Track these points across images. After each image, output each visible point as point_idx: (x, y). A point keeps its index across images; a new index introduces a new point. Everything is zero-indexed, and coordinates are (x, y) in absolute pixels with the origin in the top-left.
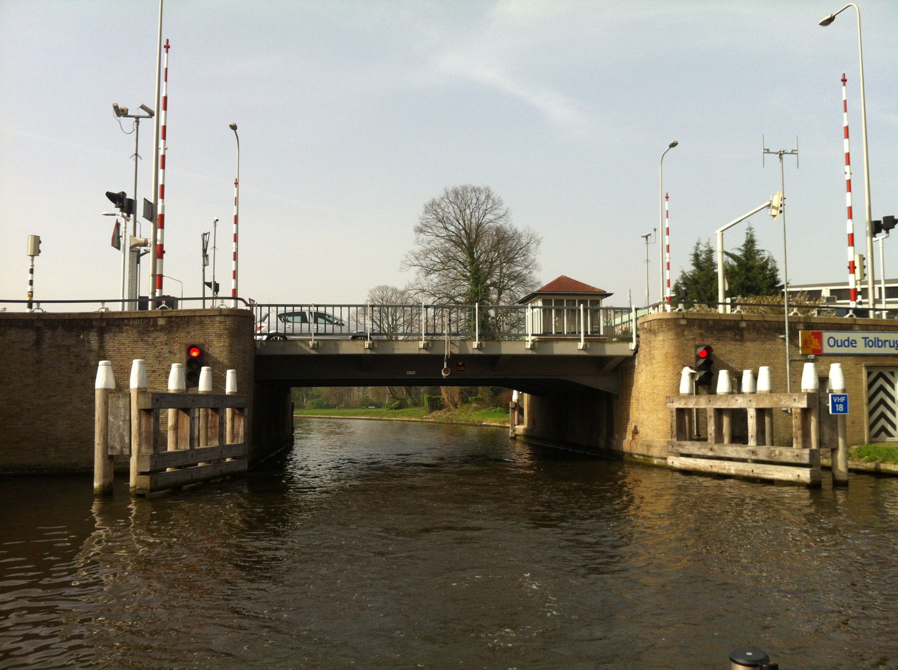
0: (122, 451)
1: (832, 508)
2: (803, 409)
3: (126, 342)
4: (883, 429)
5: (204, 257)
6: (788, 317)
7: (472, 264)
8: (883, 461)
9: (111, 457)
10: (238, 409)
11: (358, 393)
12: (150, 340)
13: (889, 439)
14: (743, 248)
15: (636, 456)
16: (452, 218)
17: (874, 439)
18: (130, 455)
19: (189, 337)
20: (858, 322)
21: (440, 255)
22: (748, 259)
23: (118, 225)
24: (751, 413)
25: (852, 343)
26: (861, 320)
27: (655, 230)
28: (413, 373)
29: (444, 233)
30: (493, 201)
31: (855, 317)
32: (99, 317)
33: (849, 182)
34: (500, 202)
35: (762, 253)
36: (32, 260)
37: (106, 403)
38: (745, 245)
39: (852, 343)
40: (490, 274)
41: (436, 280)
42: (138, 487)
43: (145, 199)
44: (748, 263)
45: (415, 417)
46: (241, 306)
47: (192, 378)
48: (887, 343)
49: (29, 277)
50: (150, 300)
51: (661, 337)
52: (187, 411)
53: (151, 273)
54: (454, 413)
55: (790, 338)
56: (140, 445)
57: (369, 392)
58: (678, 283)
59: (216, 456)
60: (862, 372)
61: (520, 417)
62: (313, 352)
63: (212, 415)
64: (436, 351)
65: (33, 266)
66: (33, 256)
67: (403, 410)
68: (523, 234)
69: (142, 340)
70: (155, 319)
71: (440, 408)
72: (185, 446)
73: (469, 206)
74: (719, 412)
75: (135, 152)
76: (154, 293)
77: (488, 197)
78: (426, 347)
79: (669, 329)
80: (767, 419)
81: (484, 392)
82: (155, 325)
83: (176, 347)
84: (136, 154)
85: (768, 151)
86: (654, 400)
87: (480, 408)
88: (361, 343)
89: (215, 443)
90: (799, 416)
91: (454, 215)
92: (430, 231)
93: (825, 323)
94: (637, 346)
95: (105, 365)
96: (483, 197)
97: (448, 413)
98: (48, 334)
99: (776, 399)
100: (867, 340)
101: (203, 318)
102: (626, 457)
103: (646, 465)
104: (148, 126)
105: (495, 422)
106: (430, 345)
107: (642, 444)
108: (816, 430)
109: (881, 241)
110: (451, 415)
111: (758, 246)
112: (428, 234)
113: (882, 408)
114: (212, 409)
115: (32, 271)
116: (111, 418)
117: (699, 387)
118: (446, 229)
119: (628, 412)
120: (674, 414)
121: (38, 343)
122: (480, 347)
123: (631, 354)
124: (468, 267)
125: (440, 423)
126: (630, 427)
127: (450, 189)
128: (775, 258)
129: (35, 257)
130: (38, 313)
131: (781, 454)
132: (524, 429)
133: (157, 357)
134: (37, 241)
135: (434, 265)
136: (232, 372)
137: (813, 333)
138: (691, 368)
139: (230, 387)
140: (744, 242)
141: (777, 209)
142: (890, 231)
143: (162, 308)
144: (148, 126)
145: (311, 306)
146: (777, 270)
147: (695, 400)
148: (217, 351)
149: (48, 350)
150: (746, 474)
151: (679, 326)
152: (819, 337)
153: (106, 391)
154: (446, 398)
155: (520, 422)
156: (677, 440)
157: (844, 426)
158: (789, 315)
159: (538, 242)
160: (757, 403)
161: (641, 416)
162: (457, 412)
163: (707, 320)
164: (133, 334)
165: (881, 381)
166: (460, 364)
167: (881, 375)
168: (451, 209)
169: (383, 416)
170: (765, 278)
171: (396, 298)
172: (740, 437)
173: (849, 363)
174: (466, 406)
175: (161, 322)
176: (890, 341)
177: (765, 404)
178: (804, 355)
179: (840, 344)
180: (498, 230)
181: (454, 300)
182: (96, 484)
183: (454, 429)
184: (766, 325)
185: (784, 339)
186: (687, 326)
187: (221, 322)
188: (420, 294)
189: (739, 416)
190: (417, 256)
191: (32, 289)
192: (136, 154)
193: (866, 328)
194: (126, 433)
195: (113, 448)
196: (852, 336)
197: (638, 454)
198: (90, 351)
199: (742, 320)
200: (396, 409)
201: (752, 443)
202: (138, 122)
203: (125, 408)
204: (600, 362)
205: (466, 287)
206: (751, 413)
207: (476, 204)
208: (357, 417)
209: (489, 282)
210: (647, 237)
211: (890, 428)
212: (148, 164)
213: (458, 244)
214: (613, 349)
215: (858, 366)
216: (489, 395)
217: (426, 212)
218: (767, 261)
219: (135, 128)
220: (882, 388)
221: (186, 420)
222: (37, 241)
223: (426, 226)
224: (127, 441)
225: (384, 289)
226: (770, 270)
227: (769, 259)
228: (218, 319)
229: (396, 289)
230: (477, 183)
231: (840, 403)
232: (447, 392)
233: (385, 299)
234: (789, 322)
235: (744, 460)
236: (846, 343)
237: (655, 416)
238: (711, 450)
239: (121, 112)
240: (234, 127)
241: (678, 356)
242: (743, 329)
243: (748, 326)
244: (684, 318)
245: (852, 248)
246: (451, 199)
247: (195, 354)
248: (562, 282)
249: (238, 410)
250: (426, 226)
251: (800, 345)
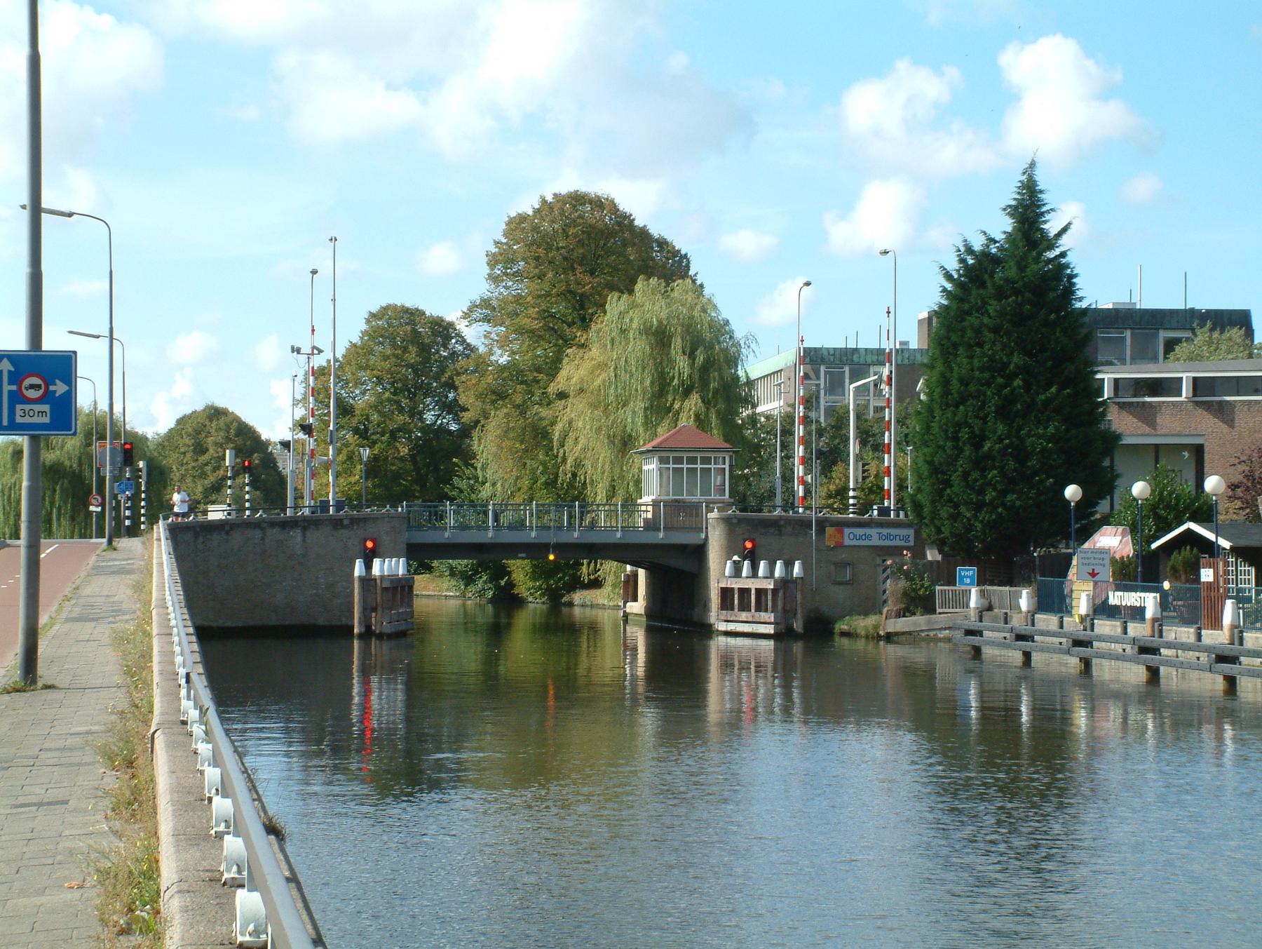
25: (868, 537)
39: (868, 537)
69: (333, 536)
123: (702, 542)
147: (480, 620)
152: (842, 533)
172: (744, 607)
196: (868, 531)
231: (967, 577)
236: (864, 537)
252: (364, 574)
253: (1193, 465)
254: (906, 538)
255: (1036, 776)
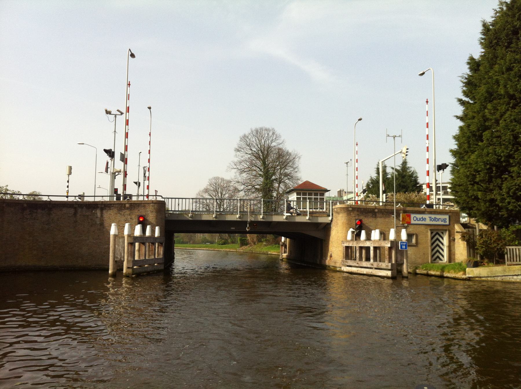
0: (121, 259)
1: (400, 286)
2: (389, 247)
3: (112, 214)
4: (438, 257)
5: (144, 177)
6: (396, 208)
7: (264, 168)
8: (430, 270)
9: (116, 261)
10: (160, 243)
11: (199, 236)
12: (122, 213)
13: (440, 262)
14: (401, 166)
15: (331, 267)
16: (254, 144)
17: (434, 261)
18: (124, 260)
19: (139, 212)
20: (427, 210)
21: (248, 164)
22: (403, 172)
23: (107, 163)
24: (372, 249)
25: (424, 219)
26: (429, 210)
27: (351, 160)
28: (234, 228)
29: (250, 152)
30: (276, 135)
31: (426, 208)
32: (101, 203)
33: (428, 148)
34: (280, 136)
35: (411, 168)
36: (69, 177)
37: (115, 240)
38: (402, 164)
39: (424, 219)
40: (274, 174)
41: (246, 176)
42: (127, 273)
43: (121, 153)
44: (403, 173)
45: (233, 249)
46: (159, 199)
47: (144, 230)
48: (440, 220)
49: (67, 184)
50: (122, 196)
51: (341, 215)
52: (144, 244)
53: (122, 184)
54: (254, 247)
55: (396, 216)
56: (128, 257)
57: (207, 236)
58: (369, 182)
59: (151, 262)
60: (428, 232)
61: (285, 249)
62: (191, 219)
63: (151, 246)
64: (244, 219)
65: (69, 179)
66: (69, 175)
67: (227, 245)
68: (292, 153)
69: (119, 213)
70: (125, 204)
71: (247, 244)
72: (142, 258)
73: (263, 138)
74: (361, 248)
75: (114, 130)
76: (123, 193)
77: (273, 133)
78: (240, 218)
79: (344, 212)
80: (378, 251)
81: (270, 237)
82: (125, 207)
83: (133, 216)
84: (115, 131)
85: (389, 136)
86: (338, 243)
87: (267, 245)
88: (212, 215)
89: (153, 257)
90: (388, 250)
91: (255, 142)
92: (243, 150)
93: (412, 210)
94: (332, 219)
95: (115, 225)
96: (271, 134)
97: (250, 247)
98: (79, 210)
99: (380, 243)
100: (431, 218)
101: (145, 204)
102: (327, 268)
103: (335, 271)
104: (121, 120)
105: (275, 252)
106: (242, 217)
107: (333, 262)
108: (395, 256)
109: (441, 174)
110: (252, 248)
111: (408, 165)
112: (241, 152)
113: (438, 248)
114: (151, 243)
115: (68, 182)
116: (116, 246)
117: (357, 237)
118: (251, 150)
119: (328, 248)
120: (344, 249)
121: (75, 214)
122: (263, 218)
123: (330, 222)
124: (262, 170)
125: (246, 252)
126: (329, 255)
127: (254, 129)
128: (417, 171)
129: (70, 175)
130: (76, 201)
131: (381, 265)
132: (286, 256)
133: (126, 221)
134: (70, 168)
135: (245, 169)
136: (158, 228)
137: (407, 215)
138: (353, 229)
139: (157, 234)
140: (401, 163)
141: (405, 154)
142: (445, 170)
143: (128, 200)
144: (121, 120)
145: (190, 199)
146: (418, 177)
148: (151, 218)
149: (79, 217)
150: (369, 273)
151: (349, 210)
153: (115, 236)
154: (249, 239)
155: (285, 252)
156: (345, 260)
157: (407, 254)
158: (397, 207)
159: (300, 158)
160: (374, 245)
161: (333, 249)
162: (255, 247)
163: (361, 208)
164: (115, 211)
165: (437, 236)
166: (255, 225)
167: (437, 233)
168: (254, 140)
169: (215, 248)
170: (411, 181)
171: (224, 183)
172: (368, 259)
173: (423, 228)
174: (260, 244)
175: (127, 205)
176: (441, 219)
177: (377, 245)
178: (403, 224)
179: (418, 220)
180: (279, 149)
181: (255, 188)
182: (110, 272)
183: (254, 256)
184: (386, 211)
185: (394, 217)
186: (352, 211)
187: (152, 206)
188: (237, 184)
189: (368, 249)
190: (236, 163)
191: (68, 189)
192: (115, 131)
193: (430, 213)
194: (122, 252)
195: (117, 258)
196: (424, 216)
197: (332, 266)
198: (97, 217)
199: (376, 209)
200: (222, 244)
201: (372, 260)
202: (116, 117)
203: (122, 242)
204: (317, 225)
205: (261, 180)
206: (372, 249)
207: (267, 137)
208: (201, 249)
209: (273, 177)
210: (347, 163)
211: (441, 257)
212: (121, 135)
213: (258, 158)
214: (322, 220)
215: (426, 229)
216: (272, 238)
217: (241, 141)
218: (413, 172)
219: (115, 119)
220: (438, 239)
221: (143, 247)
222: (70, 168)
223: (241, 148)
224: (123, 255)
225: (217, 178)
226: (414, 177)
227: (414, 171)
228: (151, 204)
229: (223, 179)
230: (268, 126)
231: (404, 245)
232: (250, 236)
233: (217, 184)
234: (396, 210)
235: (370, 268)
236: (421, 219)
237: (338, 249)
238: (358, 263)
239: (108, 112)
240: (150, 108)
241: (348, 224)
242: (376, 212)
243: (378, 211)
244: (351, 207)
245: (428, 176)
246: (254, 134)
247: (141, 219)
248: (307, 183)
249: (161, 244)
250: (241, 148)
251: (401, 220)
252: (117, 234)
253: (373, 277)
254: (444, 220)
255: (475, 146)
